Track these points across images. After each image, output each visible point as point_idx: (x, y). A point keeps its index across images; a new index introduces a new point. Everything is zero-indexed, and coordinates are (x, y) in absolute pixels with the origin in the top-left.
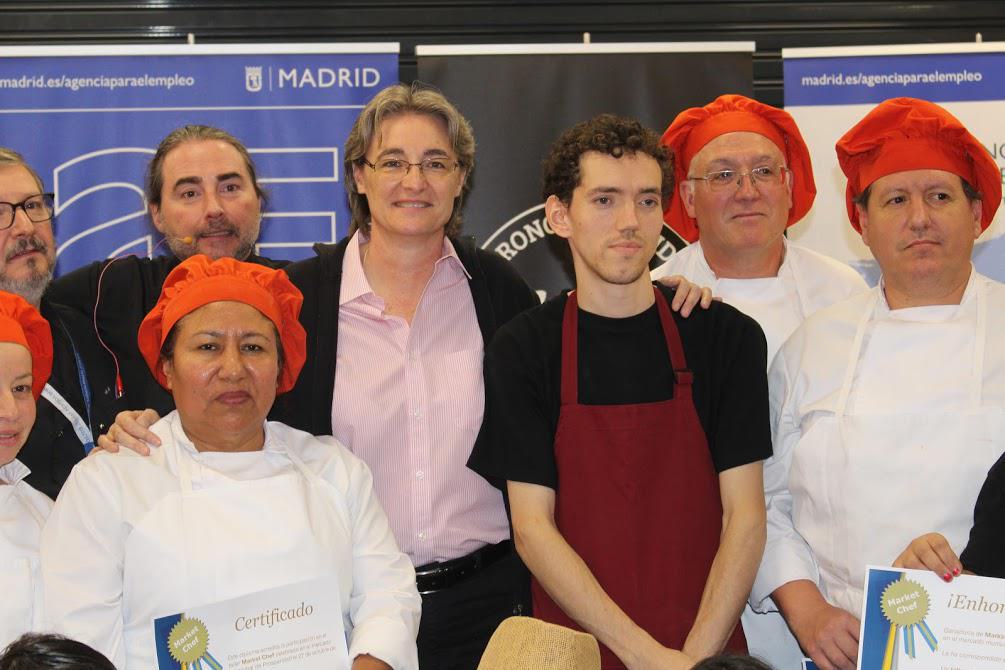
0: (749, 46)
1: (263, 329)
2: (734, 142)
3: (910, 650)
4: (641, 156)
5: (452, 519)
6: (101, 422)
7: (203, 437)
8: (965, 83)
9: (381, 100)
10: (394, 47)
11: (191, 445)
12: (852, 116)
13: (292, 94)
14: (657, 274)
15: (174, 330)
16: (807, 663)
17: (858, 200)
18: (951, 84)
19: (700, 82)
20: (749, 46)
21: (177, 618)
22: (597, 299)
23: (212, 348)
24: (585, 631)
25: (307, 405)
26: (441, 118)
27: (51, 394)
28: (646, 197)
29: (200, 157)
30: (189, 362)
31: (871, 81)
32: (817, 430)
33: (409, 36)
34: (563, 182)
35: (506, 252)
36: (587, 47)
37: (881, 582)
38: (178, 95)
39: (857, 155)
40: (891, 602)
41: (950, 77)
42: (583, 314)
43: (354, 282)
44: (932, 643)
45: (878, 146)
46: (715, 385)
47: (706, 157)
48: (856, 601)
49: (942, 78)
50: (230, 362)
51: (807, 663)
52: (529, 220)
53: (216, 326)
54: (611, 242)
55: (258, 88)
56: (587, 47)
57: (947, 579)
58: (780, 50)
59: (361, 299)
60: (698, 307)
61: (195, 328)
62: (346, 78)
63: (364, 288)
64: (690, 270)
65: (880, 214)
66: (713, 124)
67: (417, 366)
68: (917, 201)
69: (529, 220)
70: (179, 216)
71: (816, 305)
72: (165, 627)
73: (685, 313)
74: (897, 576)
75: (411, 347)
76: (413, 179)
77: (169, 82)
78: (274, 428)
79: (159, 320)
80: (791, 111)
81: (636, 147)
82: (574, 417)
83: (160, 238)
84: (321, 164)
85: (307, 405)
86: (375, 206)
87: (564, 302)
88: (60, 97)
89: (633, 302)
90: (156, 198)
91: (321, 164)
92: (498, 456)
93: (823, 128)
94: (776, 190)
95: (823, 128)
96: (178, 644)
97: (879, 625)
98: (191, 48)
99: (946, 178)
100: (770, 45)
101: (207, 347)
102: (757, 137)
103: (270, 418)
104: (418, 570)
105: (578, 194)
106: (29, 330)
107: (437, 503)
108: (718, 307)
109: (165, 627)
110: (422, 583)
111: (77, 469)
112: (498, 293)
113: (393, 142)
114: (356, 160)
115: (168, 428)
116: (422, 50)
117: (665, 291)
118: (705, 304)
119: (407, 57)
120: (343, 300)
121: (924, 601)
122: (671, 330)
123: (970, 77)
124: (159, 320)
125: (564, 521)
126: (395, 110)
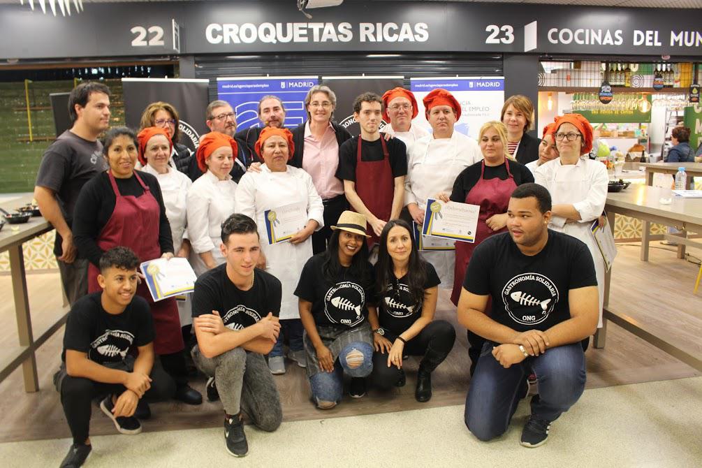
0: (403, 77)
1: (285, 142)
2: (398, 98)
3: (436, 218)
4: (376, 102)
5: (331, 189)
6: (248, 165)
7: (273, 169)
8: (454, 87)
9: (312, 89)
10: (317, 77)
11: (270, 170)
12: (426, 94)
13: (292, 89)
14: (381, 131)
15: (263, 144)
16: (175, 155)
17: (428, 112)
18: (451, 87)
19: (395, 84)
20: (403, 77)
21: (270, 211)
22: (364, 136)
23: (273, 146)
24: (356, 212)
25: (296, 160)
26: (327, 93)
27: (237, 160)
28: (377, 112)
29: (270, 102)
30: (267, 150)
31: (240, 87)
32: (416, 167)
33: (321, 74)
34: (358, 109)
35: (345, 126)
36: (363, 77)
37: (430, 202)
38: (265, 89)
39: (428, 102)
40: (433, 207)
41: (450, 85)
42: (362, 140)
43: (307, 133)
44: (441, 217)
45: (433, 99)
46: (395, 158)
47: (391, 103)
48: (424, 207)
49: (255, 86)
50: (277, 149)
51: (175, 155)
52: (349, 119)
53: (273, 140)
54: (370, 124)
55: (472, 87)
56: (363, 77)
57: (446, 202)
58: (210, 81)
59: (310, 136)
60: (390, 139)
61: (268, 142)
62: (370, 33)
63: (310, 134)
64: (389, 130)
65: (432, 116)
66: (394, 95)
67: (323, 154)
68: (441, 112)
69: (349, 119)
70: (265, 117)
71: (418, 137)
72: (267, 213)
73: (387, 140)
74: (434, 201)
75: (321, 148)
76: (320, 108)
77: (263, 86)
78: (288, 166)
79: (259, 143)
80: (414, 93)
81: (375, 100)
82: (361, 166)
83: (261, 122)
84: (300, 106)
85: (296, 160)
86: (312, 114)
87: (358, 138)
88: (238, 90)
89: (376, 137)
90: (260, 113)
91: (300, 106)
92: (342, 173)
93: (420, 97)
94: (410, 110)
95: (420, 97)
96: (270, 217)
97: (429, 213)
98: (268, 77)
99: (449, 108)
100: (407, 77)
101: (271, 146)
102: (404, 98)
103: (288, 164)
104: (323, 200)
105: (361, 112)
106: (232, 144)
107: (327, 186)
108: (395, 139)
109: (267, 213)
110: (324, 203)
111: (243, 176)
112: (342, 136)
113: (315, 100)
114: (307, 105)
115: (264, 167)
116: (323, 78)
117: (383, 134)
118: (392, 138)
119: (320, 79)
120: (305, 137)
121: (440, 207)
122: (383, 143)
123: (419, 86)
124: (259, 143)
125: (356, 189)
126: (315, 92)
